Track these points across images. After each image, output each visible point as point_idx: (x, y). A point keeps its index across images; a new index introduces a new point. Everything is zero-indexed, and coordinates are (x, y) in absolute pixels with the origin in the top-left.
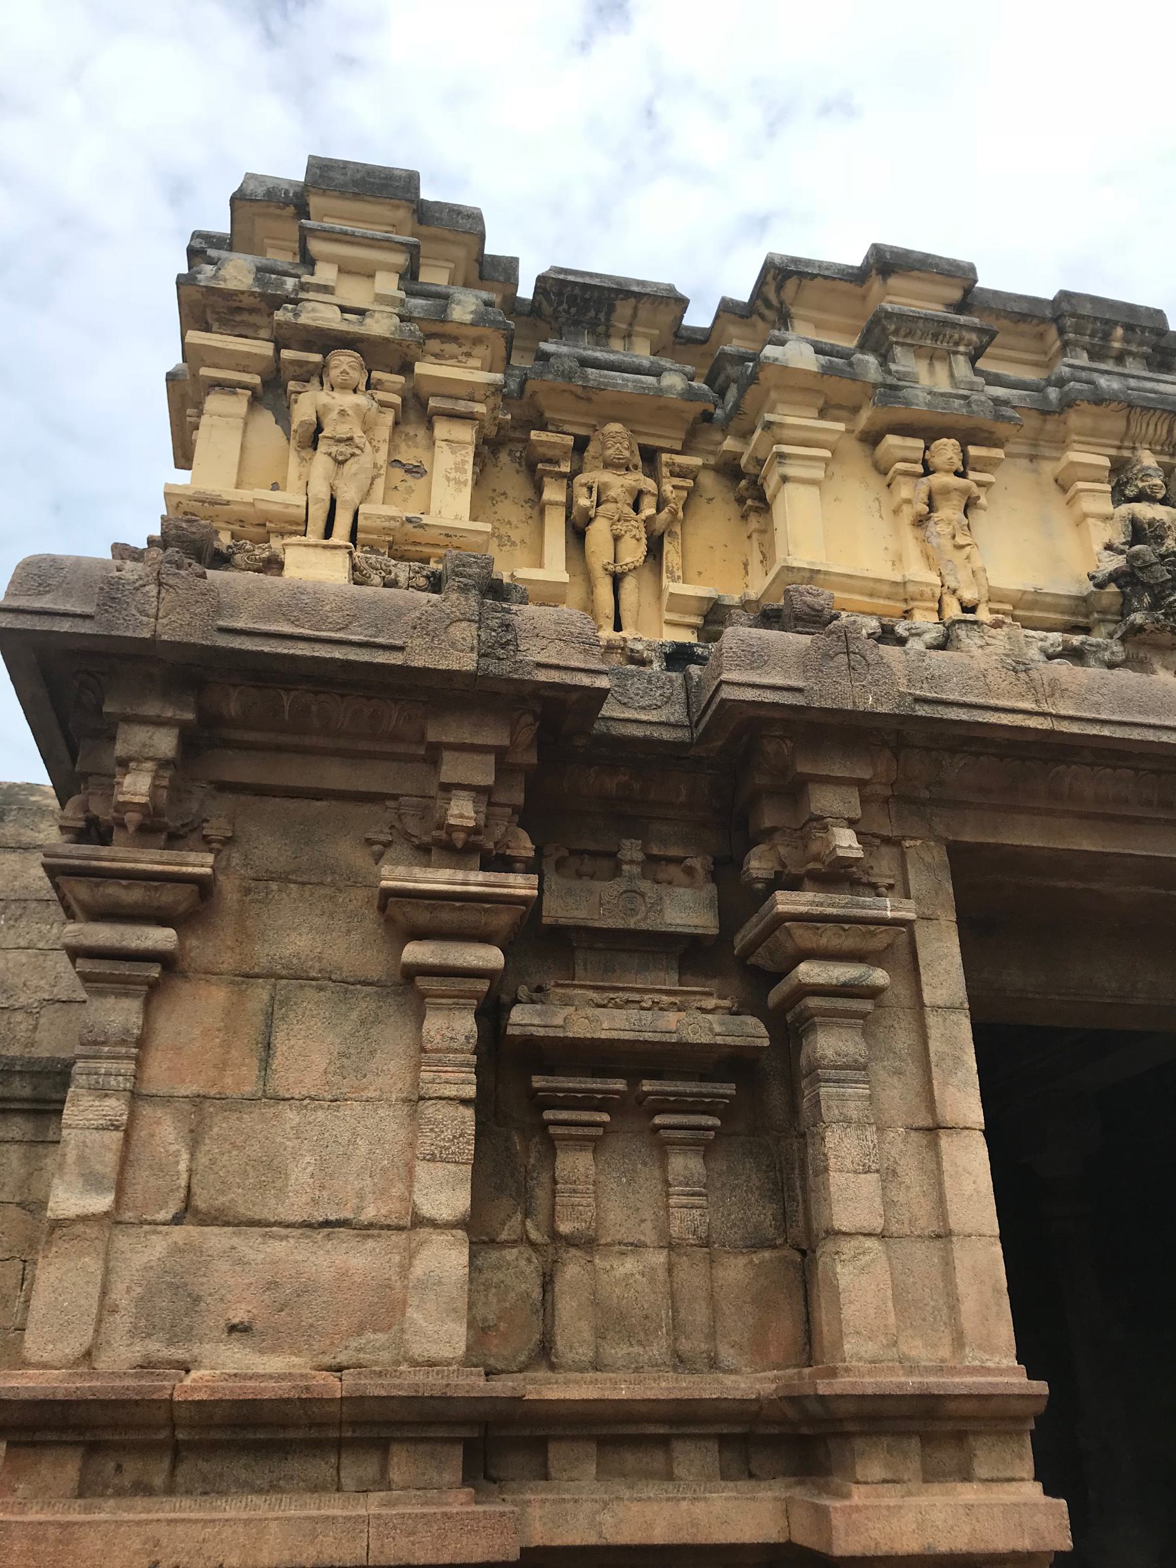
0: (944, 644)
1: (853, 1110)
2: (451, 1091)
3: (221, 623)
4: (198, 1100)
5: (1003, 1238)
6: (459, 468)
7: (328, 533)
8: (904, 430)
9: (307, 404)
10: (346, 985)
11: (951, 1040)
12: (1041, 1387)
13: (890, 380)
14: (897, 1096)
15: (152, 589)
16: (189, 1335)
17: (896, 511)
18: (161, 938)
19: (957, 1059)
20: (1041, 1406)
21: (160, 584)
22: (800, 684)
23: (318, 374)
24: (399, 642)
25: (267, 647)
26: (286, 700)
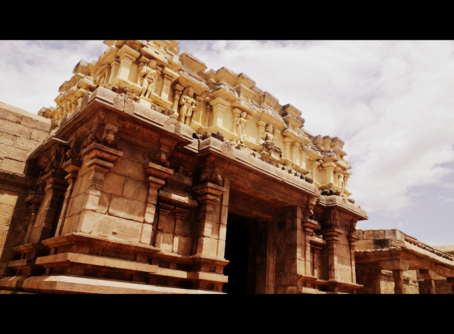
0: (238, 148)
1: (210, 218)
2: (152, 202)
3: (135, 112)
4: (111, 194)
5: (226, 241)
6: (167, 90)
7: (145, 96)
8: (239, 108)
9: (145, 69)
10: (137, 181)
11: (225, 211)
12: (228, 261)
13: (239, 99)
14: (216, 217)
15: (123, 102)
16: (106, 232)
17: (234, 122)
18: (110, 165)
19: (225, 214)
20: (227, 264)
21: (125, 101)
22: (221, 150)
23: (148, 64)
24: (163, 124)
25: (142, 119)
26: (137, 127)
